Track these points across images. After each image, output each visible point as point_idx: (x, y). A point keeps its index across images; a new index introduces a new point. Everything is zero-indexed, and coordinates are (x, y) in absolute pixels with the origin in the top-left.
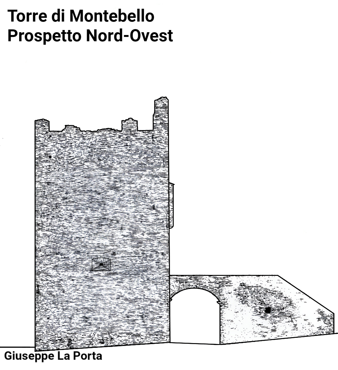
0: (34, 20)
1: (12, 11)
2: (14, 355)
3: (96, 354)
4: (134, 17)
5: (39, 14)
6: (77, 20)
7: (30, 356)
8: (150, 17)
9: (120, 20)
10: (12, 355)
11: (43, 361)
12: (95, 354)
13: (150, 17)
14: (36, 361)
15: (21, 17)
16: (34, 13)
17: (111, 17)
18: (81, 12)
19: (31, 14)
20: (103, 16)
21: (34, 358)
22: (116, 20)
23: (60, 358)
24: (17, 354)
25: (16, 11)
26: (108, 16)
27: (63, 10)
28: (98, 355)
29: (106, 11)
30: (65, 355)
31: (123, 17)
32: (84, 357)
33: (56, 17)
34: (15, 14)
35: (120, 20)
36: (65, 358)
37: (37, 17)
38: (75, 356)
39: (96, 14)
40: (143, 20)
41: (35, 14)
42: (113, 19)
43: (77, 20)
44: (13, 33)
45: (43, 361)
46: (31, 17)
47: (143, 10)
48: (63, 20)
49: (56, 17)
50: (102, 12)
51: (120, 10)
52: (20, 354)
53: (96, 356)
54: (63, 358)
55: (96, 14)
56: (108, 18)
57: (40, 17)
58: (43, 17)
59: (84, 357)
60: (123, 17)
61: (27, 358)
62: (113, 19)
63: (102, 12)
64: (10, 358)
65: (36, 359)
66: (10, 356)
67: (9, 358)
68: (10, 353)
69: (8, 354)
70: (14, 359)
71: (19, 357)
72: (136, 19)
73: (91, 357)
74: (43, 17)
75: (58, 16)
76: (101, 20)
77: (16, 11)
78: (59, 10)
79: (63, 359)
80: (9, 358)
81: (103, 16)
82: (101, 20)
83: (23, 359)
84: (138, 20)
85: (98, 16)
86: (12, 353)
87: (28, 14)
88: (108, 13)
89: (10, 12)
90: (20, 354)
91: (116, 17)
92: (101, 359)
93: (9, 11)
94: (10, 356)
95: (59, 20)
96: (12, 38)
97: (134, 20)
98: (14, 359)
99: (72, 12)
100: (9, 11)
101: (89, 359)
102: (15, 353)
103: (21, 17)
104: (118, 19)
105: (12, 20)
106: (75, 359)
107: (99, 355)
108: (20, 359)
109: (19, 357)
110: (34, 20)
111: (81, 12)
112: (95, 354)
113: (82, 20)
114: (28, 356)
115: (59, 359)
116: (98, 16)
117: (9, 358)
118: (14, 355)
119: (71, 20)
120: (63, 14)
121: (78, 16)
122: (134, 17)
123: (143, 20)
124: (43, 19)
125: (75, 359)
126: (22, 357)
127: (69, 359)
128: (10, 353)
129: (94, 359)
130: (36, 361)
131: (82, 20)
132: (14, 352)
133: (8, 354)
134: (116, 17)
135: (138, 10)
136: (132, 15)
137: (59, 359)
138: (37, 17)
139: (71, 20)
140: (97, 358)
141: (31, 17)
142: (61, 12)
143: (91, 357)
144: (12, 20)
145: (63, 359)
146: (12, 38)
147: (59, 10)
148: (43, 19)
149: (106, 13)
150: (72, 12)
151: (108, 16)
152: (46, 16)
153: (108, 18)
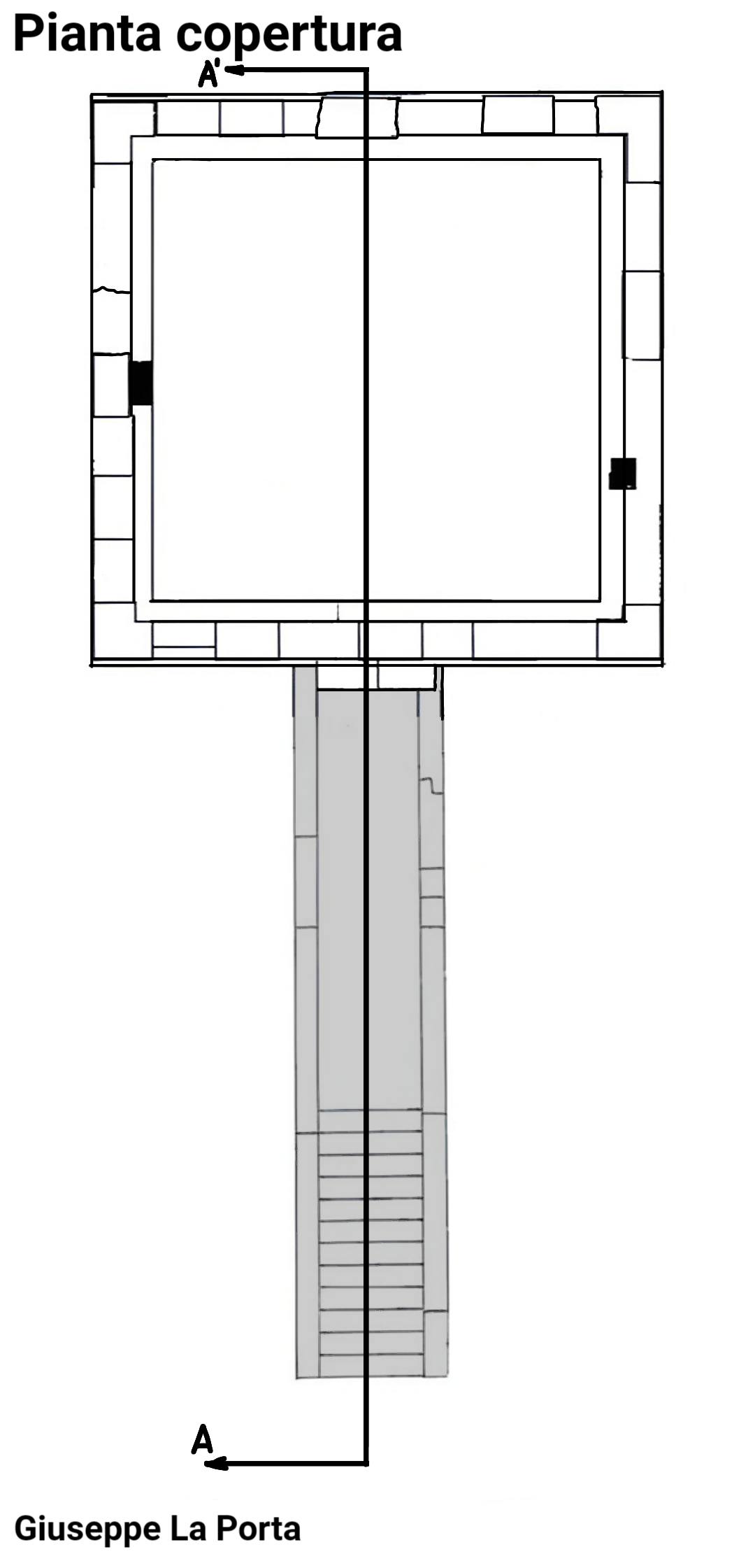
2: (42, 1525)
10: (37, 1526)
14: (107, 1545)
21: (103, 1534)
24: (51, 1525)
38: (221, 1529)
64: (33, 1536)
67: (28, 1534)
68: (32, 1521)
69: (26, 1524)
70: (42, 1538)
73: (269, 1531)
79: (185, 1538)
80: (28, 1534)
86: (38, 1521)
90: (62, 1525)
94: (32, 1530)
98: (42, 1538)
101: (262, 1538)
102: (46, 1522)
106: (220, 1538)
108: (61, 1537)
115: (175, 1537)
118: (42, 1525)
125: (220, 1538)
126: (67, 1532)
128: (32, 1521)
129: (277, 1537)
143: (269, 1531)
145: (185, 1538)
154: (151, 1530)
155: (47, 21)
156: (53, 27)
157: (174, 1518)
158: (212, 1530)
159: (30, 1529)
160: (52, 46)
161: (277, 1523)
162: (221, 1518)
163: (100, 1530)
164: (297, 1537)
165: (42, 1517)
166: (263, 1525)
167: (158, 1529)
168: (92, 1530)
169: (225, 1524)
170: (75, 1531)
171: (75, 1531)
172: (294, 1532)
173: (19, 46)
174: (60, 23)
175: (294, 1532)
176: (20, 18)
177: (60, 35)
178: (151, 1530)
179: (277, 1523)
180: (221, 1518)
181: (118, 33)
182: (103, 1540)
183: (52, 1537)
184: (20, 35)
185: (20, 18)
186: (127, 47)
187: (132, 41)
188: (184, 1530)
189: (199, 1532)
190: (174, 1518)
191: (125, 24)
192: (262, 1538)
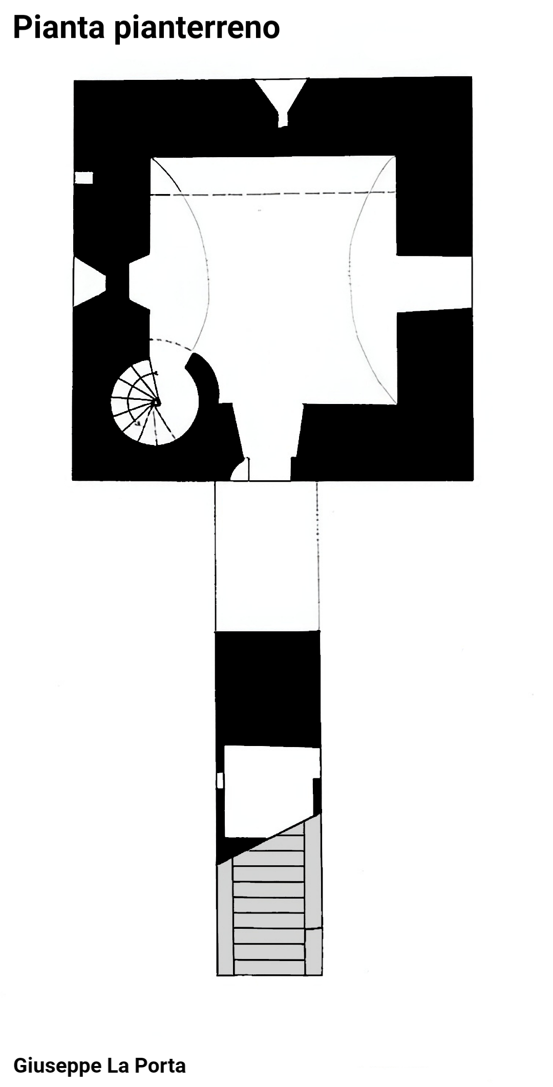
2: (30, 1063)
3: (89, 23)
7: (58, 1067)
10: (27, 1064)
11: (81, 1075)
12: (86, 23)
14: (70, 1075)
17: (190, 29)
20: (176, 27)
21: (67, 1069)
24: (36, 1063)
28: (92, 24)
32: (154, 1067)
38: (138, 1066)
42: (196, 33)
44: (141, 1063)
45: (81, 1075)
52: (42, 1063)
53: (175, 1067)
54: (117, 1069)
59: (154, 1067)
61: (53, 1070)
62: (196, 33)
64: (24, 1070)
65: (70, 1071)
66: (24, 1067)
67: (22, 1069)
68: (24, 1061)
69: (20, 1063)
70: (30, 1071)
71: (39, 1068)
73: (167, 1067)
79: (116, 1071)
80: (22, 1069)
81: (176, 27)
86: (28, 1061)
88: (184, 23)
90: (42, 1063)
92: (184, 1071)
94: (24, 1067)
96: (140, 1069)
98: (30, 1071)
101: (162, 1071)
102: (33, 1061)
106: (137, 1071)
107: (97, 26)
108: (42, 1071)
109: (39, 1068)
112: (86, 23)
114: (55, 1066)
115: (110, 1071)
118: (30, 1063)
125: (137, 1071)
126: (45, 1067)
127: (127, 1071)
128: (24, 1061)
129: (172, 1071)
130: (70, 1075)
132: (30, 1058)
137: (110, 1071)
143: (167, 1067)
145: (116, 1071)
146: (140, 1069)
149: (181, 22)
154: (96, 1067)
155: (34, 20)
156: (38, 24)
157: (110, 1060)
158: (132, 1066)
159: (22, 1066)
160: (38, 36)
161: (171, 1062)
162: (138, 1060)
163: (65, 1066)
164: (184, 1071)
165: (30, 1058)
166: (163, 1064)
167: (100, 1066)
168: (60, 1067)
169: (140, 1063)
170: (49, 1067)
171: (49, 1067)
172: (182, 1068)
173: (17, 35)
174: (42, 21)
175: (182, 1068)
176: (17, 18)
177: (42, 28)
178: (96, 1067)
179: (171, 1062)
180: (138, 1060)
181: (78, 27)
182: (67, 1072)
183: (37, 1071)
184: (18, 28)
185: (17, 18)
186: (83, 36)
187: (87, 32)
188: (115, 1067)
189: (124, 1068)
190: (110, 1060)
191: (82, 22)
192: (162, 1071)
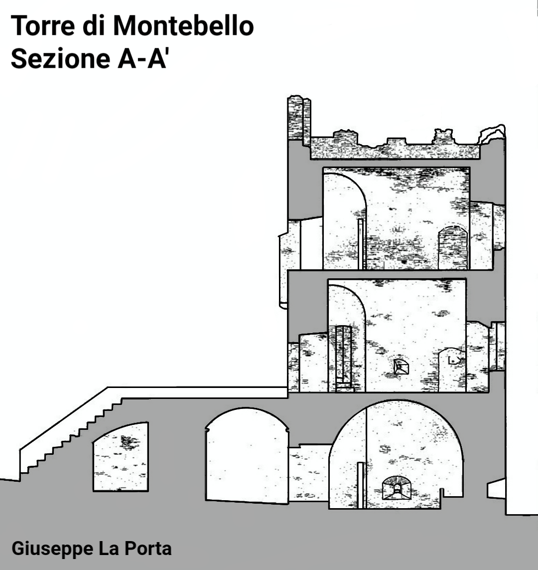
0: (54, 33)
1: (19, 18)
2: (27, 546)
4: (221, 27)
5: (62, 23)
6: (125, 32)
7: (53, 550)
8: (247, 28)
9: (197, 33)
10: (24, 547)
13: (247, 28)
15: (33, 28)
16: (54, 21)
18: (132, 18)
19: (49, 22)
20: (169, 26)
22: (190, 33)
23: (104, 552)
24: (32, 546)
25: (25, 17)
26: (177, 26)
27: (102, 16)
29: (173, 18)
30: (111, 547)
31: (201, 28)
32: (142, 550)
33: (90, 28)
34: (24, 22)
35: (197, 33)
36: (111, 551)
37: (59, 27)
38: (127, 549)
39: (156, 23)
40: (235, 33)
41: (55, 23)
42: (186, 31)
43: (125, 32)
46: (49, 27)
47: (235, 16)
48: (102, 33)
49: (90, 28)
50: (167, 19)
51: (196, 16)
52: (38, 546)
55: (156, 23)
56: (177, 30)
57: (64, 28)
58: (67, 27)
59: (142, 550)
60: (201, 28)
63: (167, 19)
65: (64, 553)
67: (19, 551)
68: (22, 544)
69: (18, 546)
71: (35, 551)
72: (224, 31)
73: (154, 550)
74: (67, 27)
75: (94, 26)
76: (165, 33)
77: (25, 17)
78: (94, 16)
81: (169, 26)
82: (165, 33)
83: (43, 553)
84: (227, 33)
85: (161, 26)
86: (25, 544)
87: (45, 23)
89: (16, 20)
90: (38, 546)
91: (190, 27)
92: (170, 553)
93: (13, 17)
94: (22, 549)
95: (94, 32)
97: (220, 33)
99: (117, 19)
100: (13, 17)
101: (150, 554)
102: (29, 544)
103: (33, 28)
104: (193, 31)
105: (19, 33)
106: (127, 554)
109: (35, 551)
110: (54, 33)
111: (132, 18)
113: (133, 33)
114: (50, 549)
115: (101, 553)
116: (161, 26)
117: (19, 551)
118: (27, 546)
119: (116, 33)
120: (102, 23)
121: (127, 25)
122: (221, 27)
123: (235, 33)
124: (68, 31)
125: (127, 554)
126: (41, 550)
127: (117, 553)
128: (22, 544)
129: (159, 553)
131: (133, 33)
132: (27, 542)
133: (18, 546)
134: (190, 27)
135: (227, 16)
136: (216, 25)
137: (101, 553)
138: (59, 27)
139: (116, 33)
140: (164, 551)
141: (49, 27)
142: (98, 19)
143: (154, 550)
144: (19, 33)
145: (107, 554)
147: (94, 16)
148: (68, 31)
149: (173, 21)
150: (117, 19)
151: (177, 26)
152: (72, 27)
153: (177, 30)
